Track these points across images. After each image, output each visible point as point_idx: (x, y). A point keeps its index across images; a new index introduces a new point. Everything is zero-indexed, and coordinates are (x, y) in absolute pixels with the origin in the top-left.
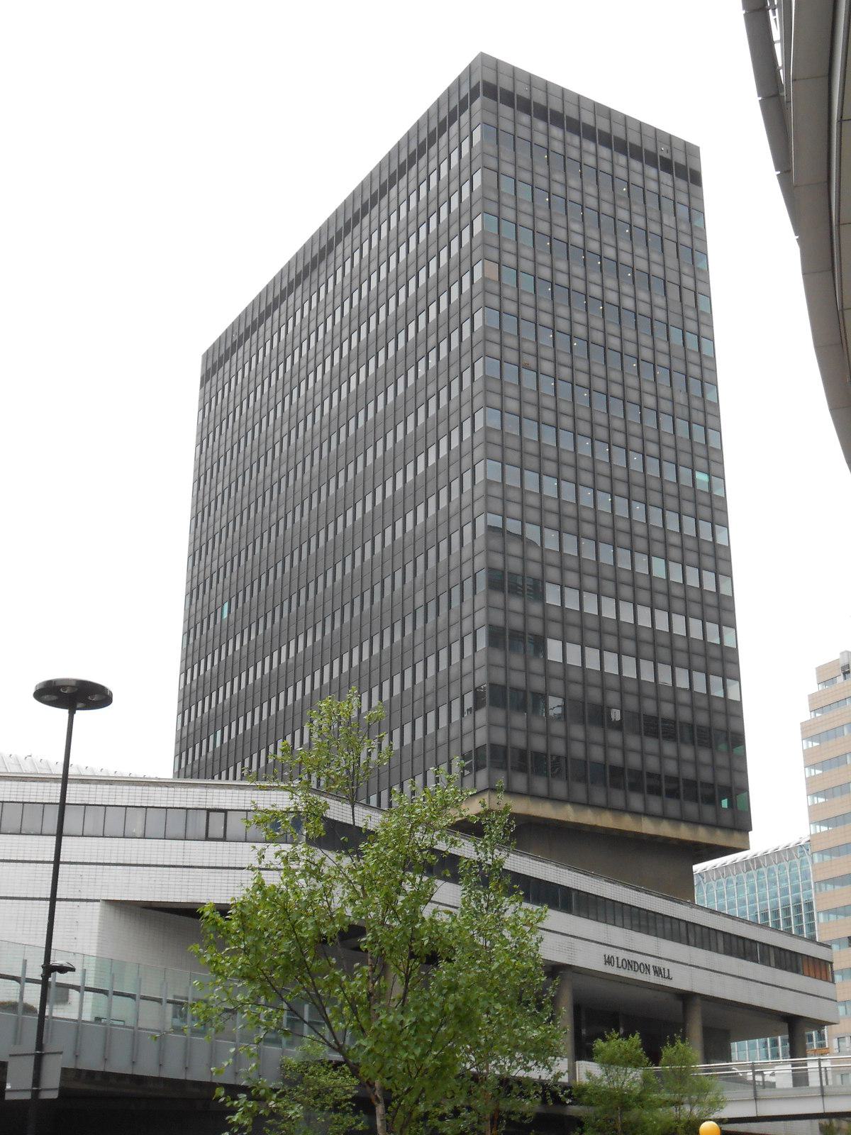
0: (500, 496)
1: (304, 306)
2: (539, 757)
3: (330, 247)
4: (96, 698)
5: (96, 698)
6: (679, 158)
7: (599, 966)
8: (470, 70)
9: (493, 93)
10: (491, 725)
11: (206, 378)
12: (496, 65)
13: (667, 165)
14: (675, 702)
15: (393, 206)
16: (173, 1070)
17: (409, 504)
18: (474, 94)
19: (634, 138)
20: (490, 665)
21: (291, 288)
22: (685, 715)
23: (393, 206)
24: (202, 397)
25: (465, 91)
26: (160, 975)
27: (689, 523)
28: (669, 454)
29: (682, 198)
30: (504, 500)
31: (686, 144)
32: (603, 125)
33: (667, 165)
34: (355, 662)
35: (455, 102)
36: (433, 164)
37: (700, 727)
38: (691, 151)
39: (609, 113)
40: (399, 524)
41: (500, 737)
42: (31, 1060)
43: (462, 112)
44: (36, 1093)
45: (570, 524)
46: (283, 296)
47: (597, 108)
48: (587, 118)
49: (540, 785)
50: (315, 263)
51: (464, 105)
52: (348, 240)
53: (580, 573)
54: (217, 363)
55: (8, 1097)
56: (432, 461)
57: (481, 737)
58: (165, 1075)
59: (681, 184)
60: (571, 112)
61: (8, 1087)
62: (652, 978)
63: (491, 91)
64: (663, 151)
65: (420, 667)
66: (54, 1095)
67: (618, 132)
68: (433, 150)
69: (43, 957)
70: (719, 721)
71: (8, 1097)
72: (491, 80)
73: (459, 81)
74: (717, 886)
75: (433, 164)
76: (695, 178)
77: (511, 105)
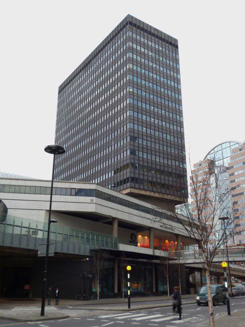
0: (133, 120)
1: (84, 76)
2: (137, 179)
3: (91, 61)
4: (61, 151)
5: (61, 151)
6: (173, 42)
7: (160, 228)
8: (126, 18)
9: (130, 24)
10: (131, 172)
11: (59, 92)
12: (132, 17)
13: (171, 43)
14: (172, 169)
15: (106, 51)
16: (65, 251)
17: (103, 126)
18: (127, 24)
19: (163, 37)
20: (131, 158)
21: (81, 71)
22: (174, 171)
23: (106, 51)
24: (59, 97)
25: (125, 23)
26: (61, 229)
27: (175, 127)
28: (171, 111)
29: (174, 51)
30: (134, 120)
31: (175, 39)
32: (156, 33)
33: (171, 43)
34: (97, 158)
35: (122, 26)
36: (116, 41)
37: (154, 182)
38: (176, 41)
39: (158, 30)
40: (108, 126)
41: (133, 175)
42: (46, 246)
43: (124, 28)
44: (47, 255)
45: (149, 126)
46: (79, 73)
47: (155, 29)
48: (153, 31)
49: (137, 186)
50: (87, 65)
51: (124, 27)
52: (95, 59)
53: (151, 137)
54: (62, 89)
55: (39, 256)
56: (100, 122)
57: (128, 175)
58: (63, 252)
59: (174, 48)
60: (149, 29)
61: (39, 253)
62: (171, 231)
63: (131, 23)
64: (170, 40)
65: (113, 159)
66: (53, 255)
67: (160, 35)
68: (117, 37)
69: (75, 210)
70: (182, 173)
71: (39, 256)
72: (131, 21)
73: (123, 21)
74: (180, 210)
75: (116, 41)
76: (177, 47)
77: (135, 27)
